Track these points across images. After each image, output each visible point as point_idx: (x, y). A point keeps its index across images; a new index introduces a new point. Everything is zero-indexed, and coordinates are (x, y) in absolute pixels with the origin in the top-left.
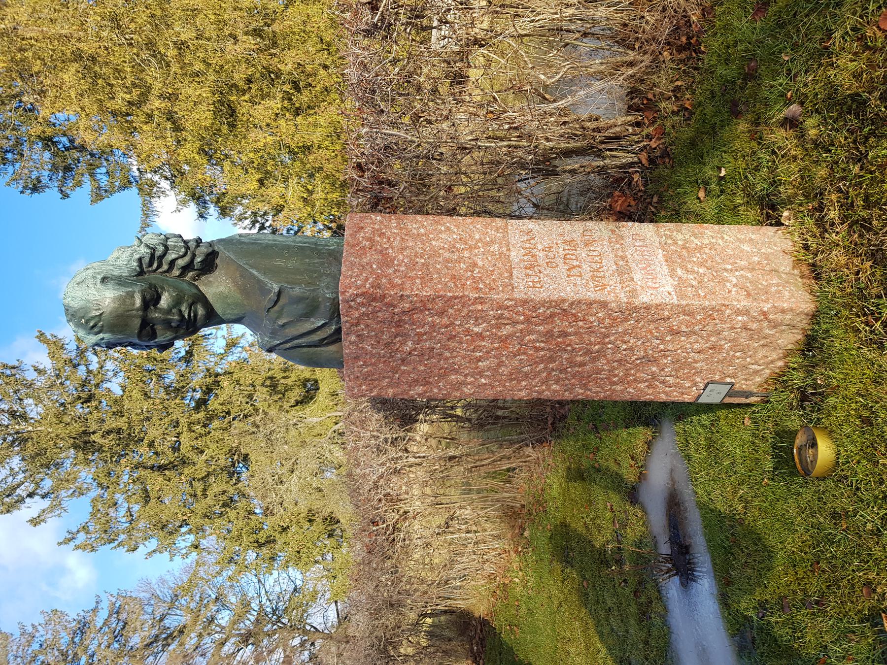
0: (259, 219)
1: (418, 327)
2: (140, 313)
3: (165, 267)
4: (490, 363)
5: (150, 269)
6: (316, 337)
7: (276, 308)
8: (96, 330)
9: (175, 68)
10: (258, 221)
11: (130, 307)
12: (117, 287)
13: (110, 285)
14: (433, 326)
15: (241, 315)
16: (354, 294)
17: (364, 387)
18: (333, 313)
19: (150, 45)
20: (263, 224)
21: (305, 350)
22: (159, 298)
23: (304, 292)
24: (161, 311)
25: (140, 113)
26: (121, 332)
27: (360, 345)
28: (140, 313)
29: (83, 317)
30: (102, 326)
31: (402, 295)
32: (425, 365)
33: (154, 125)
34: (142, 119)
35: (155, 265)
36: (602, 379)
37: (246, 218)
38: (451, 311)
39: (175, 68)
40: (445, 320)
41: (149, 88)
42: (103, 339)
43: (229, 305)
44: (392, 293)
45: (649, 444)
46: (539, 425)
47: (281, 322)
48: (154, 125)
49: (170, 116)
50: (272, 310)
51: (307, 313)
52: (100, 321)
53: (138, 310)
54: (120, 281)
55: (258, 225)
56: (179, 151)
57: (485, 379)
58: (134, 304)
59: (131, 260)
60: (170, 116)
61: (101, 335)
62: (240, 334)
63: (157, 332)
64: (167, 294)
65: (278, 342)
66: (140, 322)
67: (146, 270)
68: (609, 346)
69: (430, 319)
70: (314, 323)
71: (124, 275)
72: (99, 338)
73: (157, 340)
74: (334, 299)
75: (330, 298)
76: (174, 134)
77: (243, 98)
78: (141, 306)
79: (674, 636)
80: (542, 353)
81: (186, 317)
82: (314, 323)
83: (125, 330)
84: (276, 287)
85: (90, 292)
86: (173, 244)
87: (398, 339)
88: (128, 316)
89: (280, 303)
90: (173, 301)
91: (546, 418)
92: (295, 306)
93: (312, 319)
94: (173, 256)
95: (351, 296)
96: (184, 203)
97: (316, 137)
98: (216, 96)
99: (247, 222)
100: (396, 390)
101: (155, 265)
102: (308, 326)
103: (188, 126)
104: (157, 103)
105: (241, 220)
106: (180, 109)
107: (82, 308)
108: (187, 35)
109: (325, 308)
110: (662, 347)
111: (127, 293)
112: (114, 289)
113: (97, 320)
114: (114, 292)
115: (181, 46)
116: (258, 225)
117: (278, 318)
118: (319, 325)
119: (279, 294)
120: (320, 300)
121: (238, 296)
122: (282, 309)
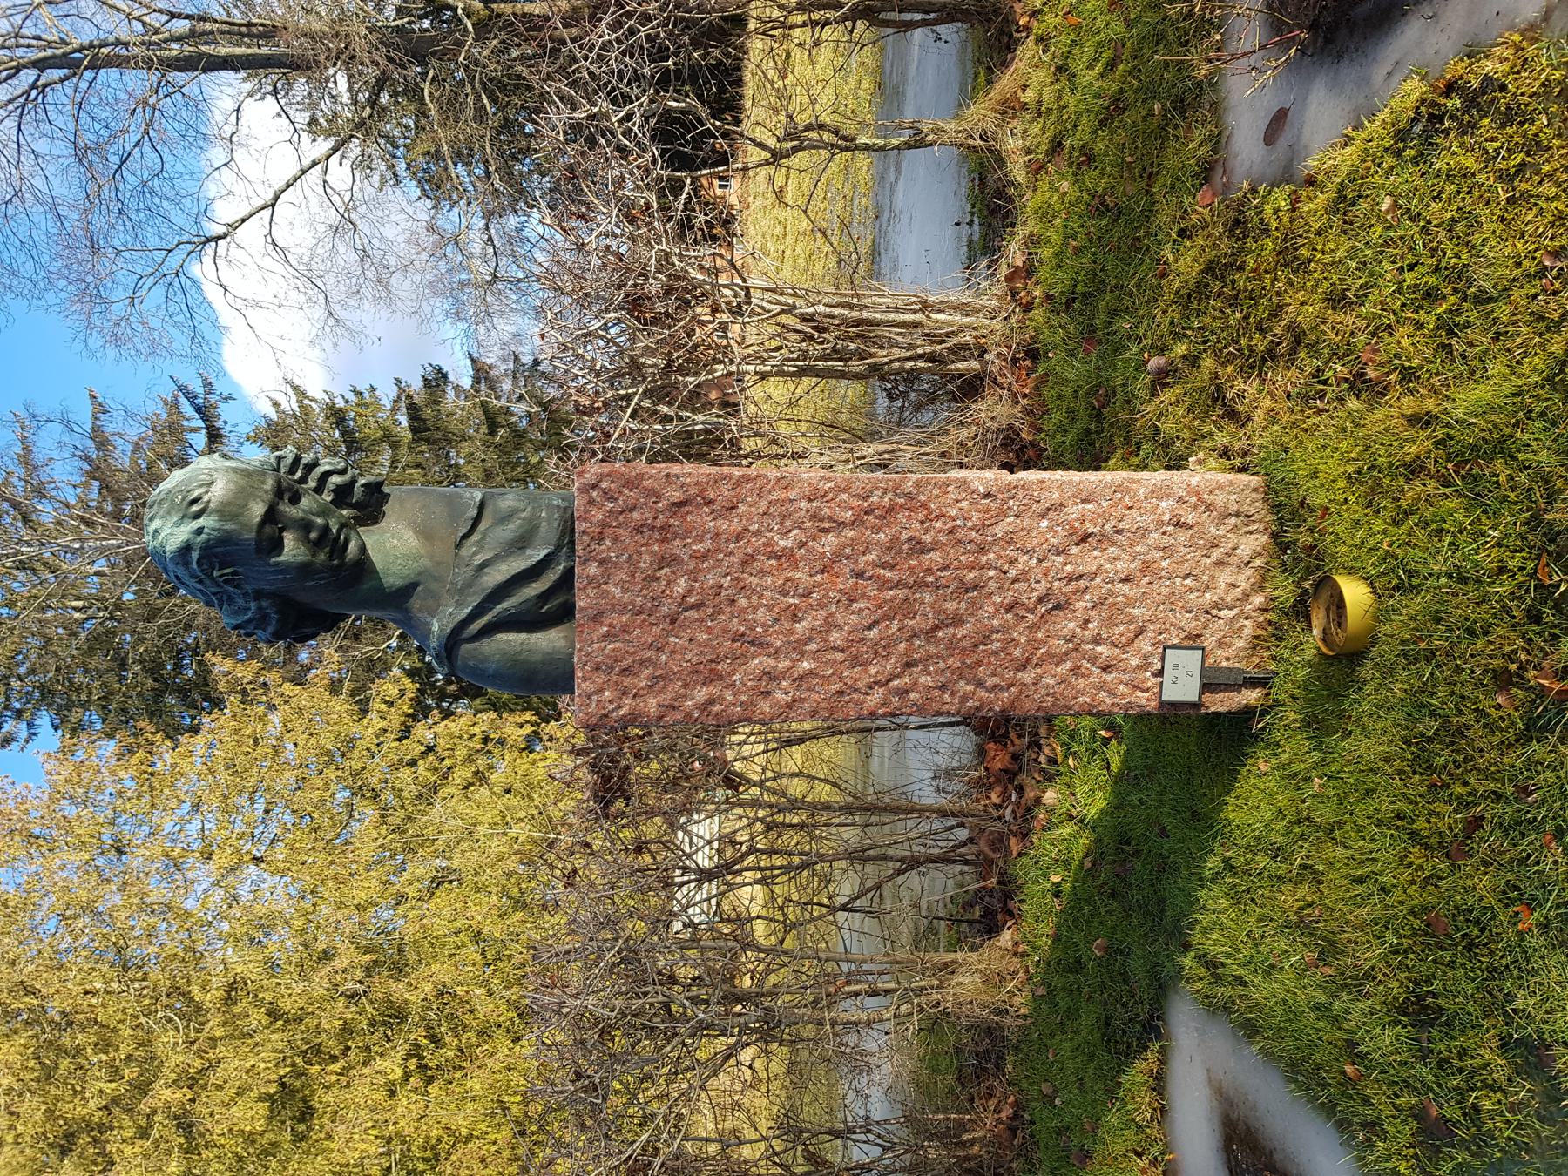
1: (694, 542)
4: (814, 619)
15: (413, 578)
17: (607, 693)
18: (563, 535)
25: (128, 1123)
31: (668, 476)
32: (709, 630)
35: (299, 474)
36: (995, 653)
40: (735, 525)
42: (199, 531)
49: (185, 1124)
60: (185, 1124)
68: (991, 573)
74: (565, 509)
75: (558, 507)
77: (331, 1067)
79: (1277, 1156)
80: (891, 593)
81: (334, 531)
82: (531, 557)
87: (663, 572)
89: (482, 527)
93: (529, 552)
97: (461, 1120)
101: (299, 474)
110: (1068, 568)
119: (481, 507)
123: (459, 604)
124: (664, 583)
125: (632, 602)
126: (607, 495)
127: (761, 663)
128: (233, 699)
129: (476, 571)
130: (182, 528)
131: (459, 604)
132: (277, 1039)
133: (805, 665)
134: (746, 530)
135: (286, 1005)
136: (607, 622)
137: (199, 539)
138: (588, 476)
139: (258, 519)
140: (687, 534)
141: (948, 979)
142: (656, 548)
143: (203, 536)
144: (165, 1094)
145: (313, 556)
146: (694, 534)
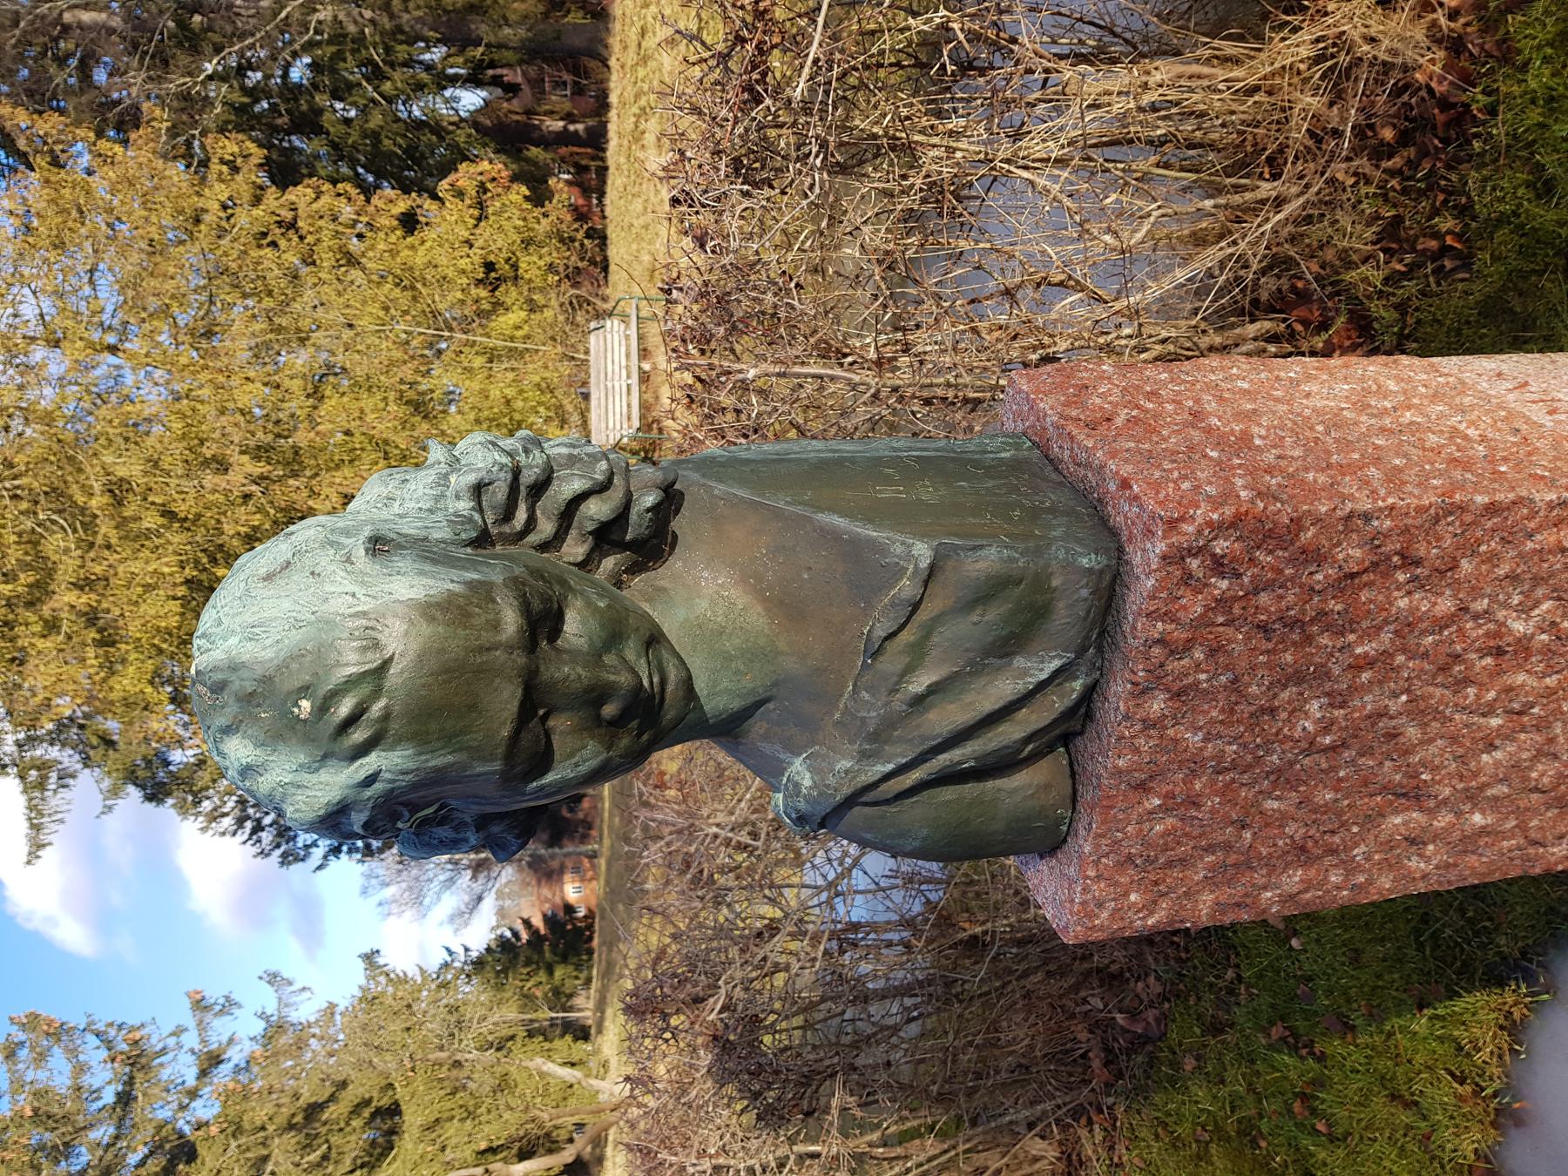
0: (251, 811)
2: (520, 659)
3: (546, 528)
5: (506, 529)
6: (1010, 732)
7: (906, 636)
8: (359, 735)
9: (106, 529)
10: (248, 817)
11: (486, 638)
12: (428, 567)
13: (404, 563)
14: (1408, 626)
16: (1210, 524)
17: (1133, 897)
19: (56, 493)
20: (259, 821)
21: (948, 793)
22: (559, 617)
23: (1011, 560)
24: (574, 654)
25: (33, 618)
26: (448, 739)
27: (1171, 732)
28: (520, 659)
29: (305, 690)
30: (386, 716)
33: (61, 638)
34: (37, 628)
37: (225, 815)
38: (1466, 566)
39: (106, 529)
41: (50, 573)
42: (370, 780)
43: (729, 658)
44: (1323, 509)
45: (1514, 1029)
46: (1070, 1075)
47: (919, 683)
48: (61, 638)
50: (892, 647)
51: (1013, 635)
52: (377, 693)
53: (509, 648)
54: (426, 552)
55: (249, 825)
56: (112, 682)
57: (1483, 812)
58: (496, 626)
59: (443, 496)
60: (91, 617)
61: (372, 762)
62: (225, 1039)
63: (556, 741)
64: (579, 603)
65: (890, 767)
66: (519, 692)
67: (494, 531)
69: (1403, 603)
70: (1025, 673)
71: (437, 535)
72: (362, 775)
73: (550, 778)
75: (1090, 570)
76: (100, 652)
78: (520, 630)
82: (1025, 673)
83: (463, 732)
84: (923, 552)
85: (328, 588)
86: (564, 450)
88: (480, 671)
89: (923, 615)
90: (603, 626)
91: (1084, 1056)
92: (975, 618)
93: (1019, 662)
94: (577, 486)
95: (1199, 532)
96: (115, 792)
98: (187, 570)
99: (227, 822)
100: (1227, 894)
102: (1004, 688)
103: (134, 629)
104: (71, 597)
105: (215, 819)
106: (112, 607)
107: (297, 656)
108: (130, 468)
109: (1066, 616)
111: (470, 584)
112: (421, 573)
113: (365, 689)
114: (425, 581)
115: (118, 491)
116: (249, 825)
117: (908, 671)
118: (1044, 676)
120: (1055, 582)
121: (756, 618)
122: (927, 636)
123: (865, 756)
124: (1284, 715)
125: (1220, 756)
126: (1219, 566)
127: (1405, 823)
128: (40, 161)
129: (911, 705)
130: (324, 776)
131: (865, 756)
132: (177, 538)
133: (1477, 818)
134: (1465, 610)
135: (181, 508)
136: (1165, 788)
137: (368, 793)
138: (1189, 528)
139: (505, 733)
140: (1350, 625)
141: (566, 66)
142: (1289, 658)
143: (378, 787)
144: (65, 599)
145: (609, 749)
146: (1365, 624)
